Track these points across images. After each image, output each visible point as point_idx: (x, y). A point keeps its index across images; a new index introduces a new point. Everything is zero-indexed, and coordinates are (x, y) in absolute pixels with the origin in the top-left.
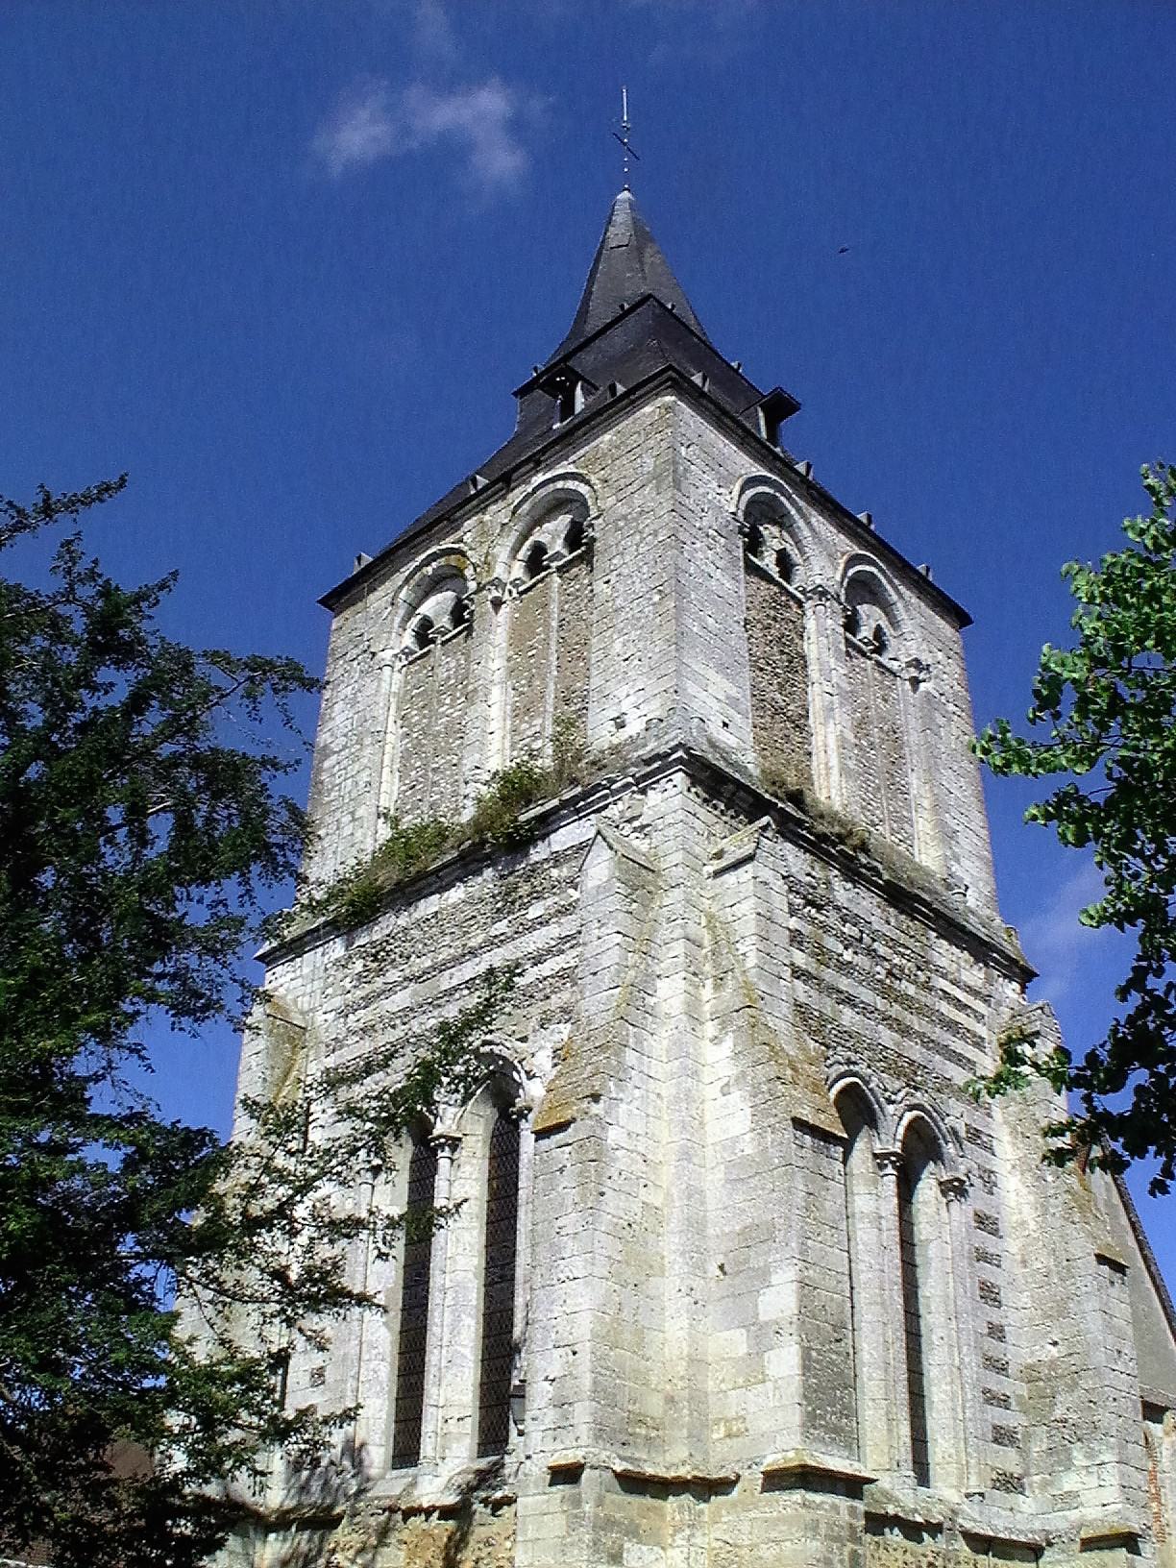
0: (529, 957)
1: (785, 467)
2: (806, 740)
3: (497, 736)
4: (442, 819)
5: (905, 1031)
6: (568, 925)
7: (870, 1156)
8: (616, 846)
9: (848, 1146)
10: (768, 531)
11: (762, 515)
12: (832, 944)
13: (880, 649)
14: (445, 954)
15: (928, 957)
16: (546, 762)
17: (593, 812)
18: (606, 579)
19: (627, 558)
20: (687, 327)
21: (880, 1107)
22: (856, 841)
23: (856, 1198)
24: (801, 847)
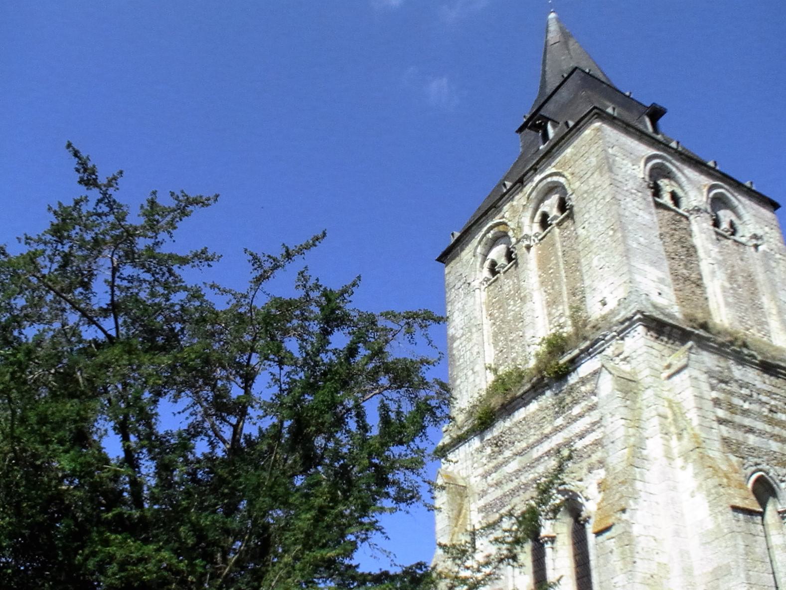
1: (664, 146)
2: (704, 292)
4: (520, 366)
6: (594, 416)
7: (776, 513)
8: (613, 372)
9: (762, 514)
10: (663, 183)
12: (737, 401)
14: (532, 440)
16: (568, 330)
18: (583, 226)
19: (592, 214)
20: (599, 80)
22: (739, 343)
23: (772, 537)
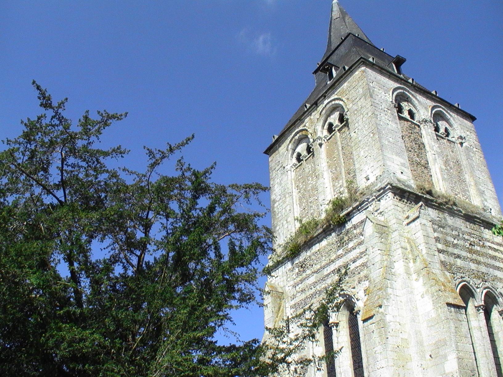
0: (351, 260)
1: (404, 81)
2: (429, 171)
3: (329, 188)
4: (316, 218)
5: (479, 263)
6: (362, 248)
7: (474, 307)
8: (373, 221)
9: (466, 308)
11: (401, 99)
12: (450, 239)
13: (448, 135)
14: (324, 263)
15: (482, 236)
17: (364, 210)
18: (354, 131)
19: (360, 124)
21: (474, 290)
22: (452, 203)
24: (434, 208)
